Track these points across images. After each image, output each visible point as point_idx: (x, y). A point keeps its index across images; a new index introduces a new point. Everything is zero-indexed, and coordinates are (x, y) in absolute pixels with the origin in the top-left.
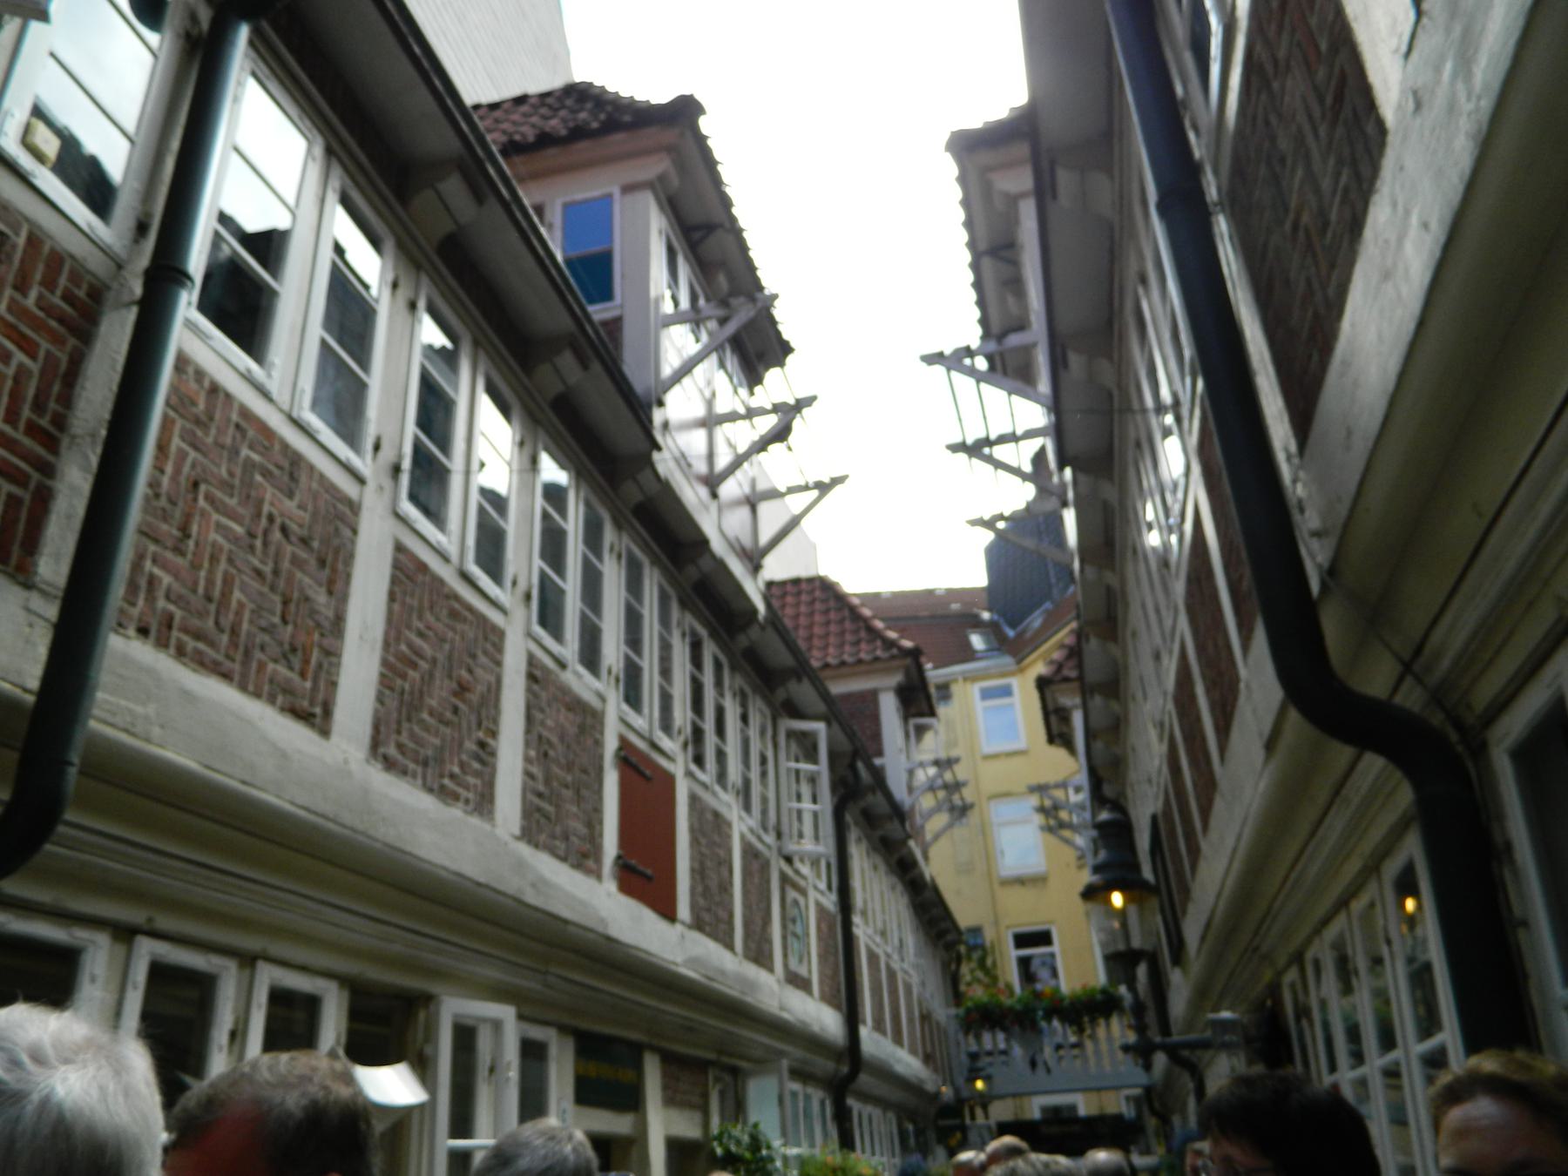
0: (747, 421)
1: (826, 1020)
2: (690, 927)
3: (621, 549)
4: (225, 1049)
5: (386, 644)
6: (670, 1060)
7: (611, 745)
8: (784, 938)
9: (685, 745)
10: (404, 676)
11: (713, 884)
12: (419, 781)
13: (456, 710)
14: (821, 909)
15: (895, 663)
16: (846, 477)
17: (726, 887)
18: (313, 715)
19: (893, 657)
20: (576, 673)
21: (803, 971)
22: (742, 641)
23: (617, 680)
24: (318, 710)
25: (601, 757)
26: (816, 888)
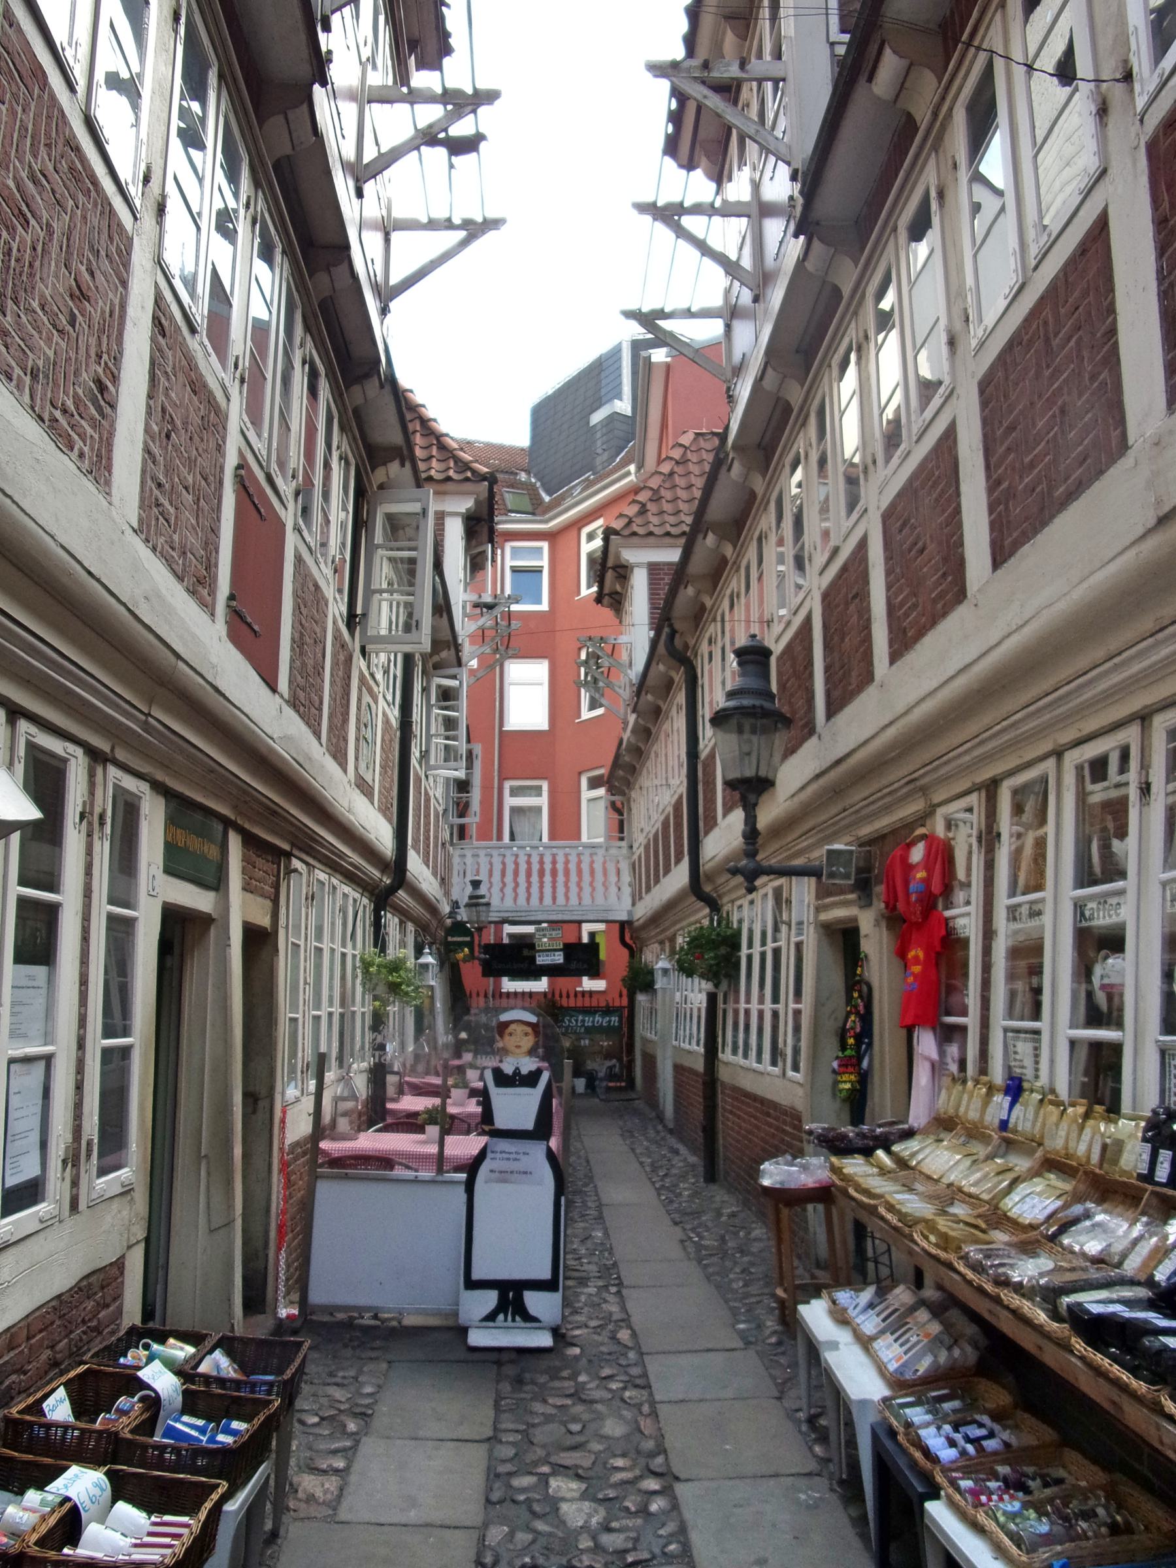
0: (407, 106)
1: (381, 833)
2: (287, 702)
6: (250, 840)
7: (231, 461)
8: (357, 739)
9: (297, 494)
10: (11, 230)
11: (310, 662)
12: (26, 398)
13: (72, 322)
14: (386, 721)
15: (469, 486)
17: (319, 673)
19: (467, 479)
20: (202, 344)
21: (368, 778)
22: (356, 395)
23: (242, 381)
25: (222, 468)
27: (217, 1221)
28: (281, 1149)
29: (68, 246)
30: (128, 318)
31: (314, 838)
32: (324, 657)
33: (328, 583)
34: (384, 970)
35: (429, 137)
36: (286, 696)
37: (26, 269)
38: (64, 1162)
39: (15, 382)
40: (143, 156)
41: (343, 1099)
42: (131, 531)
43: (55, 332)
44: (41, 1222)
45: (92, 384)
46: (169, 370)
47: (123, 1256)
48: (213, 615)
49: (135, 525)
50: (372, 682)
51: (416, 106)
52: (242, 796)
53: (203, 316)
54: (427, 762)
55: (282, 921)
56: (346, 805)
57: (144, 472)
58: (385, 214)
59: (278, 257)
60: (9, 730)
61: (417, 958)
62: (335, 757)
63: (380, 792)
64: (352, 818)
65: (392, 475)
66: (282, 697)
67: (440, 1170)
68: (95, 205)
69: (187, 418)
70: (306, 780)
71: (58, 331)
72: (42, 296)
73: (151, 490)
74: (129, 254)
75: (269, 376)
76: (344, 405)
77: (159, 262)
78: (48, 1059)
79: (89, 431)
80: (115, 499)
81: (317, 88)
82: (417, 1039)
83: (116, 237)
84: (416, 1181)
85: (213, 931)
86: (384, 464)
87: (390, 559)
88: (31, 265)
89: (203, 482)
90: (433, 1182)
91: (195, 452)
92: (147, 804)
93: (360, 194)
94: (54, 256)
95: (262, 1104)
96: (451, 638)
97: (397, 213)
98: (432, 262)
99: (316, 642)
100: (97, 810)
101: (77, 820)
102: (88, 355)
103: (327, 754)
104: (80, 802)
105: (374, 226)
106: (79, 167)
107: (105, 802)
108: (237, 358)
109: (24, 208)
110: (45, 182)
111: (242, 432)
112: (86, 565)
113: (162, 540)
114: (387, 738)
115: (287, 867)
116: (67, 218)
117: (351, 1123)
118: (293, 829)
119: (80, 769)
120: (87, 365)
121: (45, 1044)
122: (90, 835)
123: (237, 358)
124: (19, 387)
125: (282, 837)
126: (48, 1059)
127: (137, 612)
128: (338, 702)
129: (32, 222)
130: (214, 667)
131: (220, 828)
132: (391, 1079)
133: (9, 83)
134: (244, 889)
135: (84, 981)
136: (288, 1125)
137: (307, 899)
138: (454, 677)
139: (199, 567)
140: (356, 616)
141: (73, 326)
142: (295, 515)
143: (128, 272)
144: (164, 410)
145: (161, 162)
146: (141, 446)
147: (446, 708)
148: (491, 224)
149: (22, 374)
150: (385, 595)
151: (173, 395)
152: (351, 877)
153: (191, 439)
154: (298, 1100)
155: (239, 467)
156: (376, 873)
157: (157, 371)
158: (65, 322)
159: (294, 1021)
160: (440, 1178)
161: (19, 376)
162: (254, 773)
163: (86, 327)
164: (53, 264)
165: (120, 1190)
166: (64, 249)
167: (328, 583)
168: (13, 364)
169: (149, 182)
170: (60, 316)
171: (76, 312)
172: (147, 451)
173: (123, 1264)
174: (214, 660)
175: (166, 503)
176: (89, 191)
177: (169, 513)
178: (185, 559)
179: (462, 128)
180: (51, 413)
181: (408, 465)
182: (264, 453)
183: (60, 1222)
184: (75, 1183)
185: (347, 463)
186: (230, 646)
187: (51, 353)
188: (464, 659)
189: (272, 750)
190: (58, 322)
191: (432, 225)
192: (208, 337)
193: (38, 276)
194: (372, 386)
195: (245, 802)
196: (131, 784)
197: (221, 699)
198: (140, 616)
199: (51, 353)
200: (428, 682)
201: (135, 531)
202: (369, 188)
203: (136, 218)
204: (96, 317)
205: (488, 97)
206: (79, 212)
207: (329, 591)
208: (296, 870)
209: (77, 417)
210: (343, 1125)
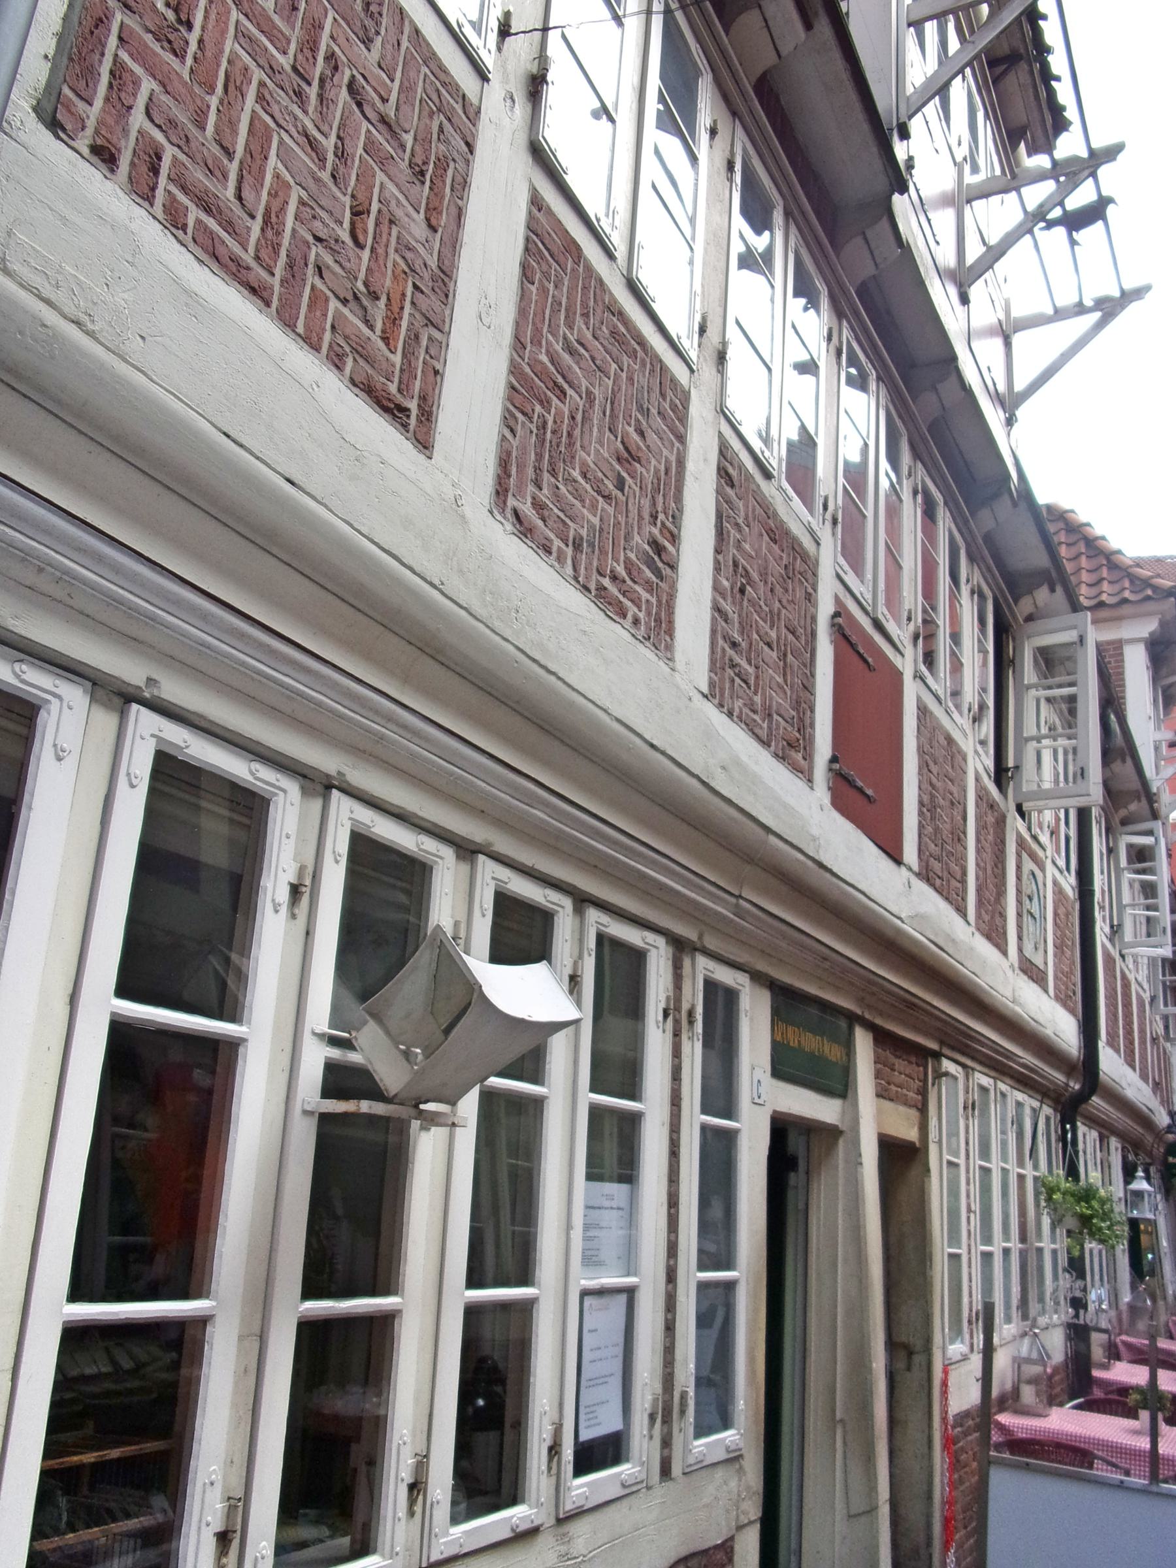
3: (841, 342)
4: (284, 910)
5: (518, 343)
6: (882, 1038)
7: (825, 609)
8: (1019, 915)
9: (916, 637)
10: (545, 403)
11: (946, 828)
12: (569, 570)
14: (1059, 891)
15: (1151, 606)
16: (1148, 288)
17: (959, 837)
18: (405, 410)
19: (1148, 598)
20: (780, 488)
21: (1038, 960)
22: (985, 520)
23: (835, 522)
24: (413, 405)
25: (814, 619)
26: (1054, 863)
27: (858, 1505)
28: (944, 1419)
29: (612, 410)
30: (688, 474)
31: (969, 1033)
32: (965, 819)
33: (965, 735)
34: (1069, 1199)
35: (1037, 217)
36: (916, 868)
37: (564, 439)
38: (652, 1417)
39: (555, 554)
40: (698, 306)
41: (1028, 1361)
42: (700, 696)
43: (600, 499)
44: (624, 1486)
45: (647, 547)
46: (740, 521)
47: (732, 1538)
48: (810, 781)
49: (705, 690)
50: (1034, 846)
51: (1024, 190)
52: (869, 987)
53: (780, 460)
54: (1122, 938)
55: (933, 1135)
56: (1009, 994)
57: (714, 632)
58: (1002, 317)
59: (873, 386)
60: (578, 920)
61: (1127, 1182)
62: (988, 937)
63: (1056, 977)
64: (1018, 1009)
65: (1040, 603)
66: (910, 869)
67: (1154, 1477)
68: (643, 364)
69: (766, 568)
70: (952, 967)
71: (603, 497)
72: (584, 464)
73: (723, 650)
74: (686, 408)
75: (869, 513)
76: (970, 531)
77: (722, 411)
78: (630, 1292)
79: (645, 595)
80: (680, 662)
81: (896, 197)
82: (1134, 1287)
83: (669, 394)
84: (1121, 1485)
85: (841, 1142)
86: (1030, 592)
87: (1048, 700)
88: (570, 435)
89: (790, 637)
90: (1143, 1491)
91: (777, 604)
92: (748, 997)
93: (964, 299)
94: (595, 422)
95: (918, 1359)
96: (1140, 787)
97: (1016, 313)
98: (1062, 355)
99: (952, 803)
100: (685, 1006)
101: (661, 1018)
102: (640, 517)
103: (977, 935)
104: (662, 998)
105: (990, 332)
106: (623, 330)
107: (694, 996)
108: (826, 499)
109: (560, 380)
110: (582, 351)
111: (838, 577)
112: (648, 737)
113: (738, 704)
114: (1062, 911)
115: (935, 1071)
116: (610, 383)
117: (1038, 1394)
118: (939, 1024)
119: (662, 962)
120: (639, 528)
121: (628, 1275)
122: (677, 1034)
123: (826, 499)
124: (560, 559)
125: (927, 1034)
126: (630, 1292)
127: (713, 784)
128: (989, 871)
129: (570, 392)
130: (814, 839)
131: (843, 1024)
132: (1097, 1339)
133: (539, 263)
134: (878, 1095)
135: (673, 1202)
136: (952, 1389)
137: (965, 1108)
138: (1150, 833)
139: (790, 729)
140: (1008, 770)
141: (622, 490)
142: (915, 661)
143: (685, 426)
144: (736, 564)
145: (720, 310)
146: (709, 604)
147: (1143, 871)
148: (1128, 297)
149: (563, 546)
150: (1045, 742)
151: (747, 547)
152: (1024, 1081)
153: (772, 590)
154: (965, 1358)
155: (837, 614)
156: (1059, 1077)
157: (725, 524)
158: (611, 487)
159: (954, 1258)
160: (1154, 1488)
161: (559, 547)
162: (880, 959)
163: (637, 489)
164: (595, 430)
165: (722, 1456)
166: (608, 413)
167: (965, 735)
168: (552, 536)
169: (705, 331)
170: (606, 481)
171: (625, 475)
172: (717, 608)
173: (732, 1548)
174: (815, 831)
175: (744, 663)
176: (635, 351)
177: (747, 673)
178: (770, 722)
179: (1082, 196)
180: (598, 581)
181: (1059, 589)
182: (869, 597)
183: (648, 1488)
184: (666, 1443)
185: (982, 596)
186: (836, 815)
187: (596, 521)
188: (1163, 811)
189: (899, 931)
190: (602, 488)
191: (1059, 314)
192: (788, 479)
193: (578, 444)
194: (1003, 507)
195: (874, 994)
196: (725, 976)
197: (828, 875)
198: (718, 788)
199: (596, 521)
200: (1116, 841)
201: (705, 696)
202: (976, 291)
203: (692, 371)
204: (649, 477)
205: (1112, 153)
206: (624, 375)
207: (967, 744)
208: (946, 1074)
209: (629, 582)
210: (1028, 1394)
